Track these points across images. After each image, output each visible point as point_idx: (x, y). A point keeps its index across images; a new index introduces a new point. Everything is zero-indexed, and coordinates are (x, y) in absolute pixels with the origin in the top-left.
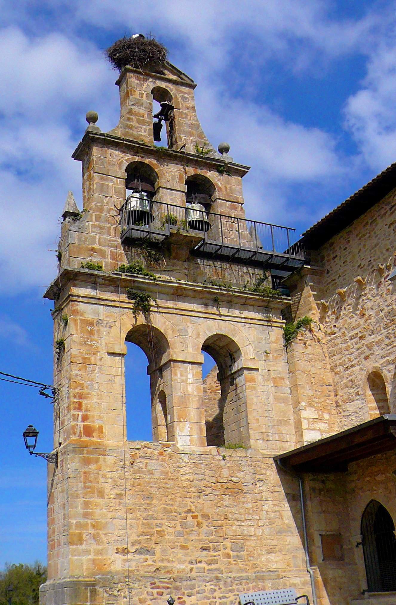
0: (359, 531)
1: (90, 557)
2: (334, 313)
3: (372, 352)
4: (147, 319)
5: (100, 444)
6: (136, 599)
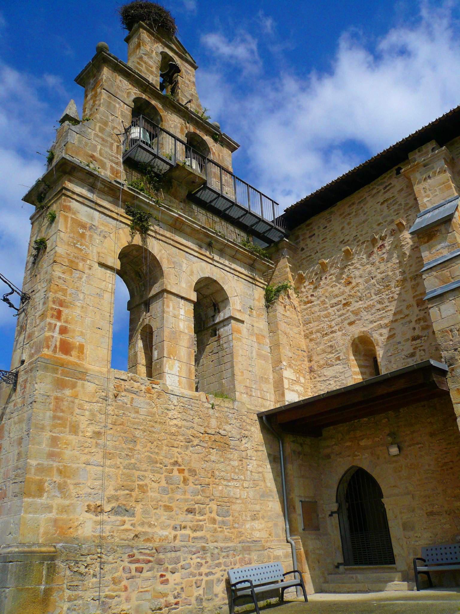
0: (334, 499)
1: (50, 515)
2: (312, 283)
3: (359, 317)
4: (144, 240)
5: (79, 366)
6: (108, 577)
